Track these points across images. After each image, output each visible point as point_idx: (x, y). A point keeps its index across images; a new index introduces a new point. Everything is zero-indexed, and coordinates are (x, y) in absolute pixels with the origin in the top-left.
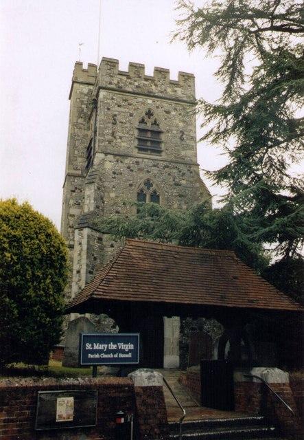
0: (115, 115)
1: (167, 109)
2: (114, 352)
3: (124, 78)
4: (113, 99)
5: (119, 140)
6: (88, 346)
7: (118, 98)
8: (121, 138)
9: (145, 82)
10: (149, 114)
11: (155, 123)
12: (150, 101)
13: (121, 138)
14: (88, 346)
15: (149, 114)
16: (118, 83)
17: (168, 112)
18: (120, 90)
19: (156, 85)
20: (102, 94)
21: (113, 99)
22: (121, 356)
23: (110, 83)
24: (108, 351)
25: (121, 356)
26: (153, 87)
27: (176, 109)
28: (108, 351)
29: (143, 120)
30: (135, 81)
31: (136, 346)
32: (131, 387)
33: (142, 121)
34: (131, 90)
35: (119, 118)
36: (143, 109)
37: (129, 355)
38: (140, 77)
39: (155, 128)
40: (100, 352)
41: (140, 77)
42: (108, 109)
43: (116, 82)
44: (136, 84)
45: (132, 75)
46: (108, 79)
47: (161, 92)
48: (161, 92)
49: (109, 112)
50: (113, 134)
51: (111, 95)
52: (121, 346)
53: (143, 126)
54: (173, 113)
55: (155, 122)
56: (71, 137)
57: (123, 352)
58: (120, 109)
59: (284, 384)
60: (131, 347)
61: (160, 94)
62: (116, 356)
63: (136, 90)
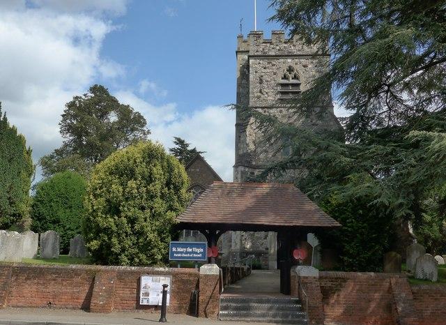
0: (262, 76)
1: (304, 63)
2: (190, 253)
3: (268, 45)
4: (259, 63)
5: (266, 95)
6: (174, 249)
7: (264, 63)
8: (267, 93)
9: (286, 45)
10: (290, 70)
11: (296, 77)
12: (289, 60)
13: (267, 93)
14: (174, 249)
15: (290, 70)
16: (263, 49)
17: (305, 66)
18: (265, 56)
19: (294, 46)
20: (251, 61)
21: (259, 63)
22: (195, 255)
23: (257, 51)
24: (187, 253)
25: (195, 255)
26: (292, 48)
27: (312, 63)
28: (187, 253)
29: (285, 76)
30: (277, 45)
31: (204, 250)
32: (197, 276)
33: (285, 77)
34: (274, 54)
35: (265, 78)
36: (285, 67)
37: (200, 255)
38: (281, 42)
39: (295, 81)
40: (181, 253)
41: (281, 42)
42: (256, 72)
43: (261, 49)
44: (278, 48)
45: (274, 41)
46: (256, 48)
47: (299, 50)
48: (299, 50)
49: (257, 74)
50: (261, 92)
51: (258, 61)
52: (195, 249)
53: (285, 81)
54: (310, 66)
55: (295, 76)
56: (136, 94)
57: (196, 253)
58: (265, 71)
59: (315, 278)
60: (202, 250)
61: (299, 53)
62: (191, 255)
63: (278, 53)
